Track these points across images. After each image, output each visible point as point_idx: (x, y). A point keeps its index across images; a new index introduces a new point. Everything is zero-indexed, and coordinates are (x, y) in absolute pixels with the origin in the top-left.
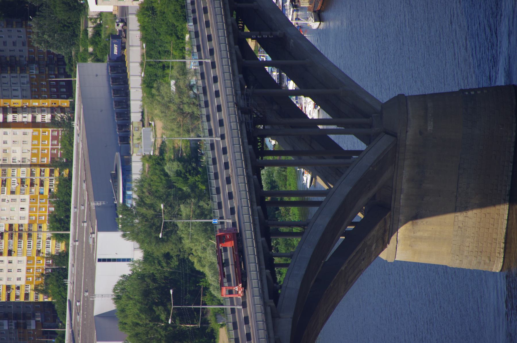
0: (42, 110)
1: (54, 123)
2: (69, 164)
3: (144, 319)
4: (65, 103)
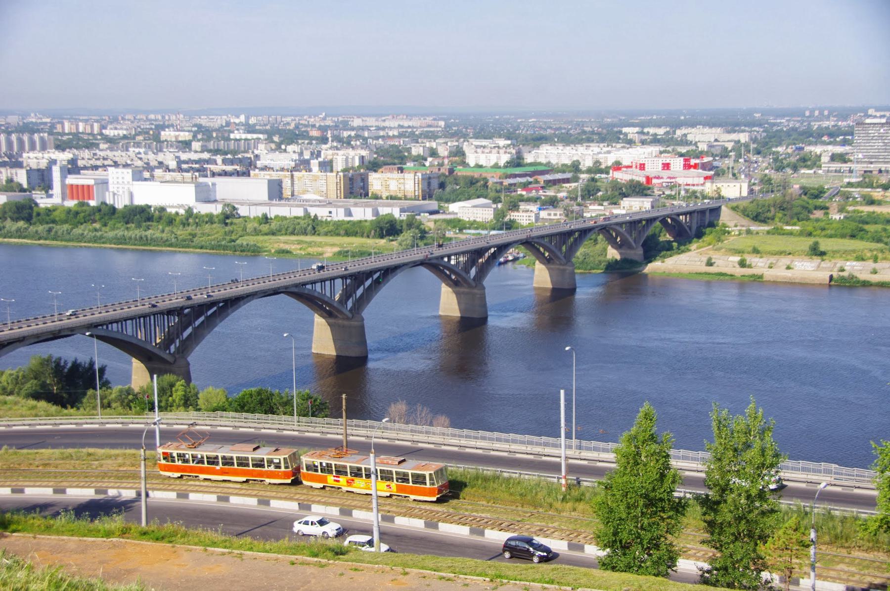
1: (415, 196)
3: (386, 221)
4: (420, 198)
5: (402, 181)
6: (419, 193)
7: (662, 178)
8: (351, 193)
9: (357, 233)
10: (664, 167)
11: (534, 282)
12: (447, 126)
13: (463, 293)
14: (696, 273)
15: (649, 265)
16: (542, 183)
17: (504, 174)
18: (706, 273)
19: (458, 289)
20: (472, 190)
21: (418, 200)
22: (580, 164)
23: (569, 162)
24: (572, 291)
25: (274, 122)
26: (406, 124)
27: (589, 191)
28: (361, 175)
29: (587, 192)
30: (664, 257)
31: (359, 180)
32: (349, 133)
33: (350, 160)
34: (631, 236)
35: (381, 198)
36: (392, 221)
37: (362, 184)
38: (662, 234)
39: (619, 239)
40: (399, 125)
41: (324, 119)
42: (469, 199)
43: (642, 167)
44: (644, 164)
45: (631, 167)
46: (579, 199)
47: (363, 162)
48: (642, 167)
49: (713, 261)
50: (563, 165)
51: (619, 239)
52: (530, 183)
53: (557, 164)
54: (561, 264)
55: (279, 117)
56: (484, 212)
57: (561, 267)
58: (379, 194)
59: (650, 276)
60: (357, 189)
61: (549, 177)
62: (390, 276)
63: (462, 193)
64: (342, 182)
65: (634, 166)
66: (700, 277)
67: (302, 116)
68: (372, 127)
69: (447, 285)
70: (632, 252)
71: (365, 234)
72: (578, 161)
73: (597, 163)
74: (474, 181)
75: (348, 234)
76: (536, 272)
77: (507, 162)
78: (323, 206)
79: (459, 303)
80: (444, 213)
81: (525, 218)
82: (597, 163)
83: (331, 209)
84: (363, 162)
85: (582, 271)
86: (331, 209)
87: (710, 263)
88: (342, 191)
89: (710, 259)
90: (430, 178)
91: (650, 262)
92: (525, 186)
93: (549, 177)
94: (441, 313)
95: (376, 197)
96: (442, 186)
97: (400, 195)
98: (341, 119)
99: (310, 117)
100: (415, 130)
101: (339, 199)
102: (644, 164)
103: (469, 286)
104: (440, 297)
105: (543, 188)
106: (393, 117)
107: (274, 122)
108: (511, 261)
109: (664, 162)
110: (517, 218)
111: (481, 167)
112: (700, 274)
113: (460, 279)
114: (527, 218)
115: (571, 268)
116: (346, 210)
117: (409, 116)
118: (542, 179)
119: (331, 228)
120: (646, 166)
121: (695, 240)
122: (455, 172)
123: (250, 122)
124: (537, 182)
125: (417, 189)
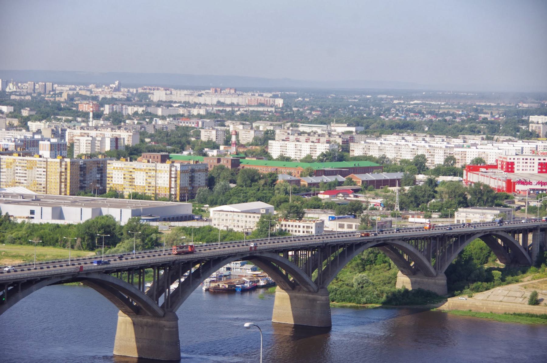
0: (176, 191)
2: (156, 200)
3: (99, 226)
4: (178, 199)
5: (153, 173)
6: (176, 191)
7: (530, 183)
8: (82, 188)
9: (57, 241)
10: (541, 169)
11: (274, 315)
12: (286, 106)
13: (147, 325)
14: (515, 314)
15: (449, 300)
16: (360, 184)
17: (308, 169)
18: (529, 315)
19: (140, 319)
20: (251, 191)
21: (177, 201)
22: (426, 160)
23: (410, 157)
24: (326, 329)
25: (42, 91)
26: (228, 101)
27: (416, 197)
28: (98, 163)
29: (413, 199)
30: (478, 290)
31: (95, 170)
32: (135, 109)
33: (98, 144)
34: (429, 260)
35: (122, 197)
36: (109, 226)
37: (98, 176)
38: (490, 259)
39: (412, 264)
40: (219, 102)
41: (117, 89)
42: (246, 201)
43: (510, 167)
44: (512, 164)
45: (495, 167)
46: (397, 207)
47: (117, 147)
48: (510, 167)
49: (539, 297)
50: (403, 161)
51: (412, 264)
52: (340, 184)
53: (395, 159)
54: (310, 292)
55: (49, 85)
56: (248, 219)
57: (311, 296)
58: (120, 189)
59: (449, 314)
60: (89, 182)
61: (370, 177)
62: (20, 294)
63: (236, 193)
64: (69, 172)
65: (499, 166)
66: (519, 320)
67: (87, 84)
68: (175, 102)
69: (124, 312)
70: (431, 281)
71: (69, 244)
72: (423, 156)
73: (450, 159)
74: (256, 177)
75: (45, 242)
76: (277, 302)
77: (323, 155)
78: (27, 203)
79: (138, 340)
80: (201, 219)
81: (301, 229)
82: (450, 159)
83: (33, 208)
84: (117, 147)
85: (354, 304)
86: (33, 208)
87: (535, 301)
88: (68, 185)
89: (535, 295)
90: (193, 171)
91: (454, 296)
92: (331, 188)
93: (370, 177)
94: (115, 353)
95: (117, 195)
96: (211, 182)
97: (149, 193)
98: (140, 90)
99: (97, 87)
100: (236, 109)
101: (63, 195)
102: (512, 164)
103: (155, 314)
104: (115, 330)
105: (356, 191)
106: (216, 91)
107: (42, 91)
108: (263, 287)
109: (542, 161)
110: (290, 228)
111: (288, 159)
112: (520, 315)
113: (141, 305)
114: (305, 230)
115: (323, 298)
116: (54, 209)
117: (239, 90)
118: (359, 179)
119: (23, 232)
120: (515, 166)
121: (533, 268)
122: (241, 165)
123: (7, 90)
124: (351, 182)
125: (173, 186)
